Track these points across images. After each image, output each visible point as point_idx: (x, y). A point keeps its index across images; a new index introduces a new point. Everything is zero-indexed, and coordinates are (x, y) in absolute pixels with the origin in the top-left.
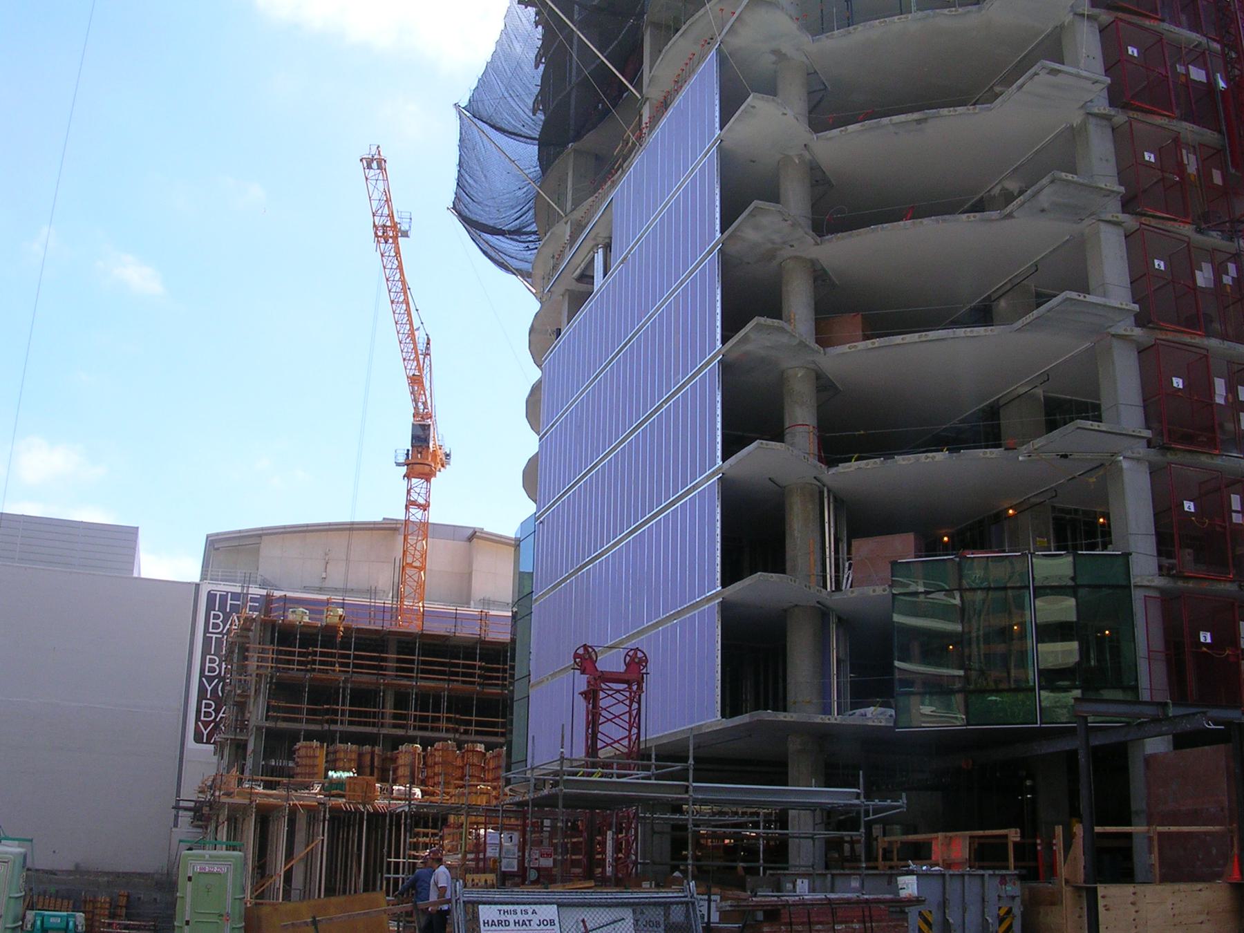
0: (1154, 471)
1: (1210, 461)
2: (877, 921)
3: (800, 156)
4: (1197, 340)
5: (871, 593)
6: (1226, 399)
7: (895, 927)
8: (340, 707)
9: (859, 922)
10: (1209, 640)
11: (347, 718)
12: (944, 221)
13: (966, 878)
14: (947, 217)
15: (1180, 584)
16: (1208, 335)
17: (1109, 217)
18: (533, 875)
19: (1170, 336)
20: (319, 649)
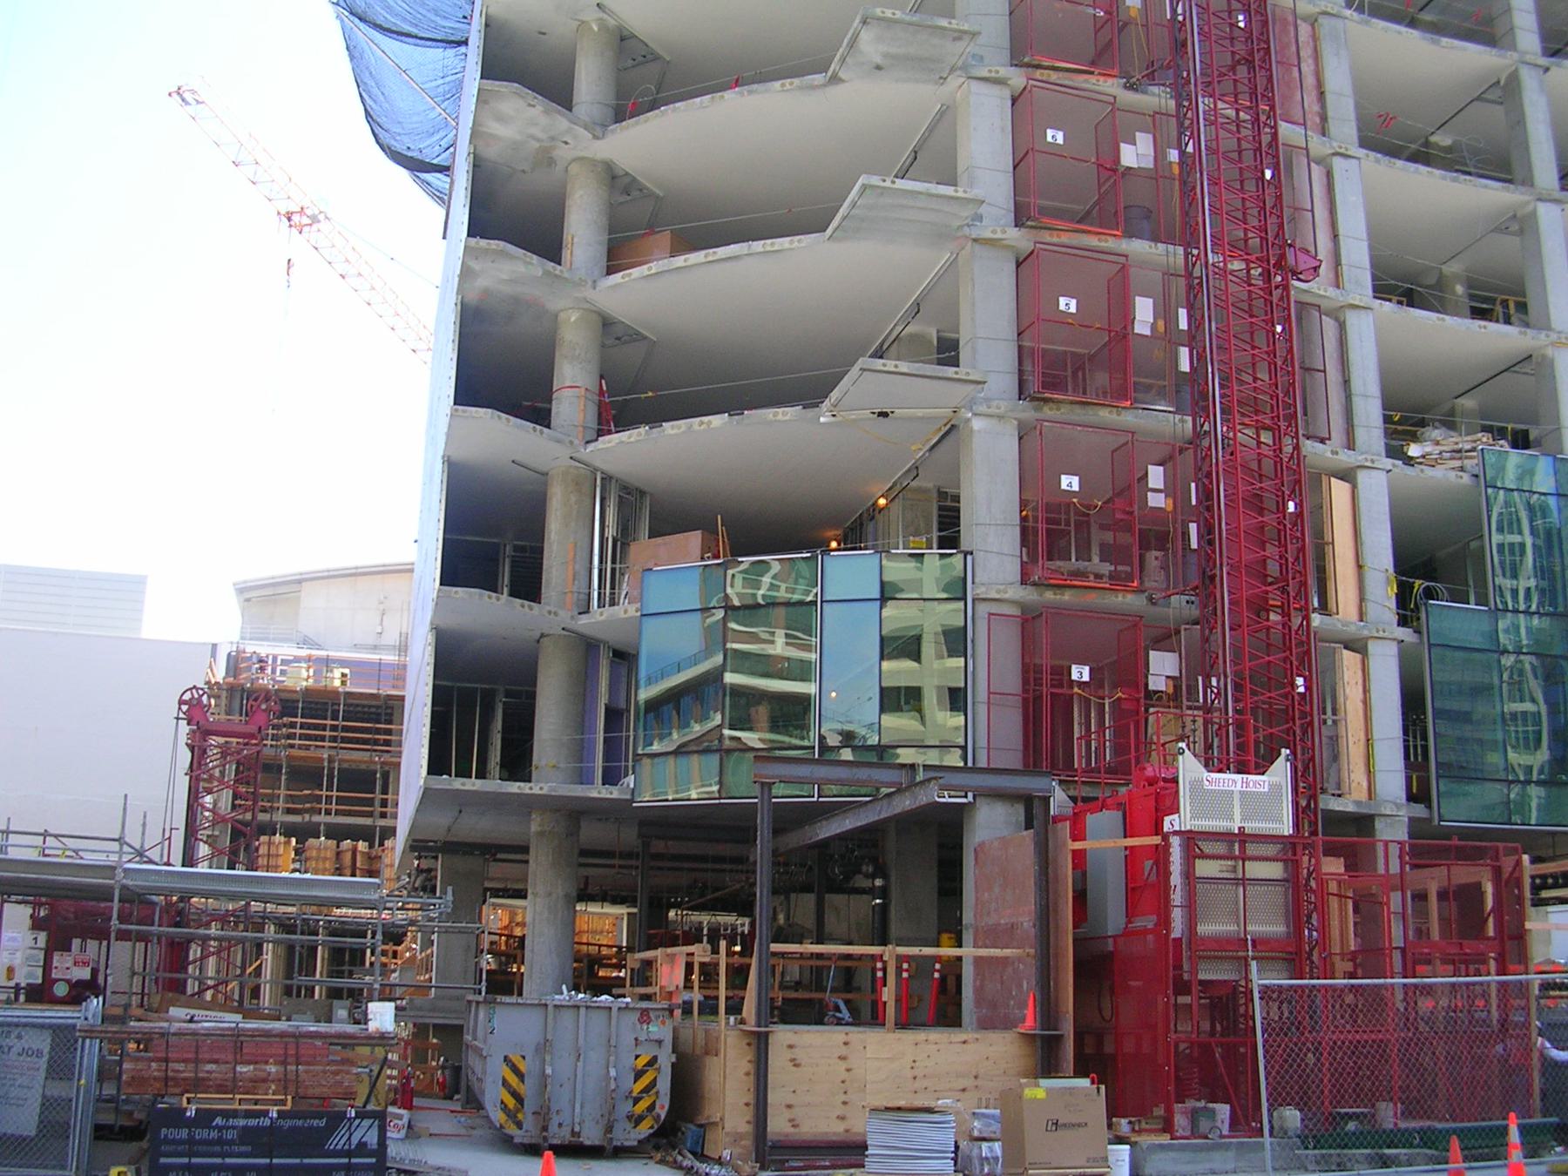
0: (1024, 434)
1: (1114, 416)
2: (308, 1064)
3: (601, 21)
4: (1110, 244)
5: (622, 615)
6: (1154, 327)
7: (336, 1073)
8: (324, 793)
9: (275, 1063)
10: (1086, 678)
11: (334, 806)
12: (750, 92)
13: (583, 1011)
14: (755, 86)
15: (1049, 595)
16: (1130, 234)
17: (985, 74)
18: (61, 990)
19: (1065, 239)
20: (299, 720)
